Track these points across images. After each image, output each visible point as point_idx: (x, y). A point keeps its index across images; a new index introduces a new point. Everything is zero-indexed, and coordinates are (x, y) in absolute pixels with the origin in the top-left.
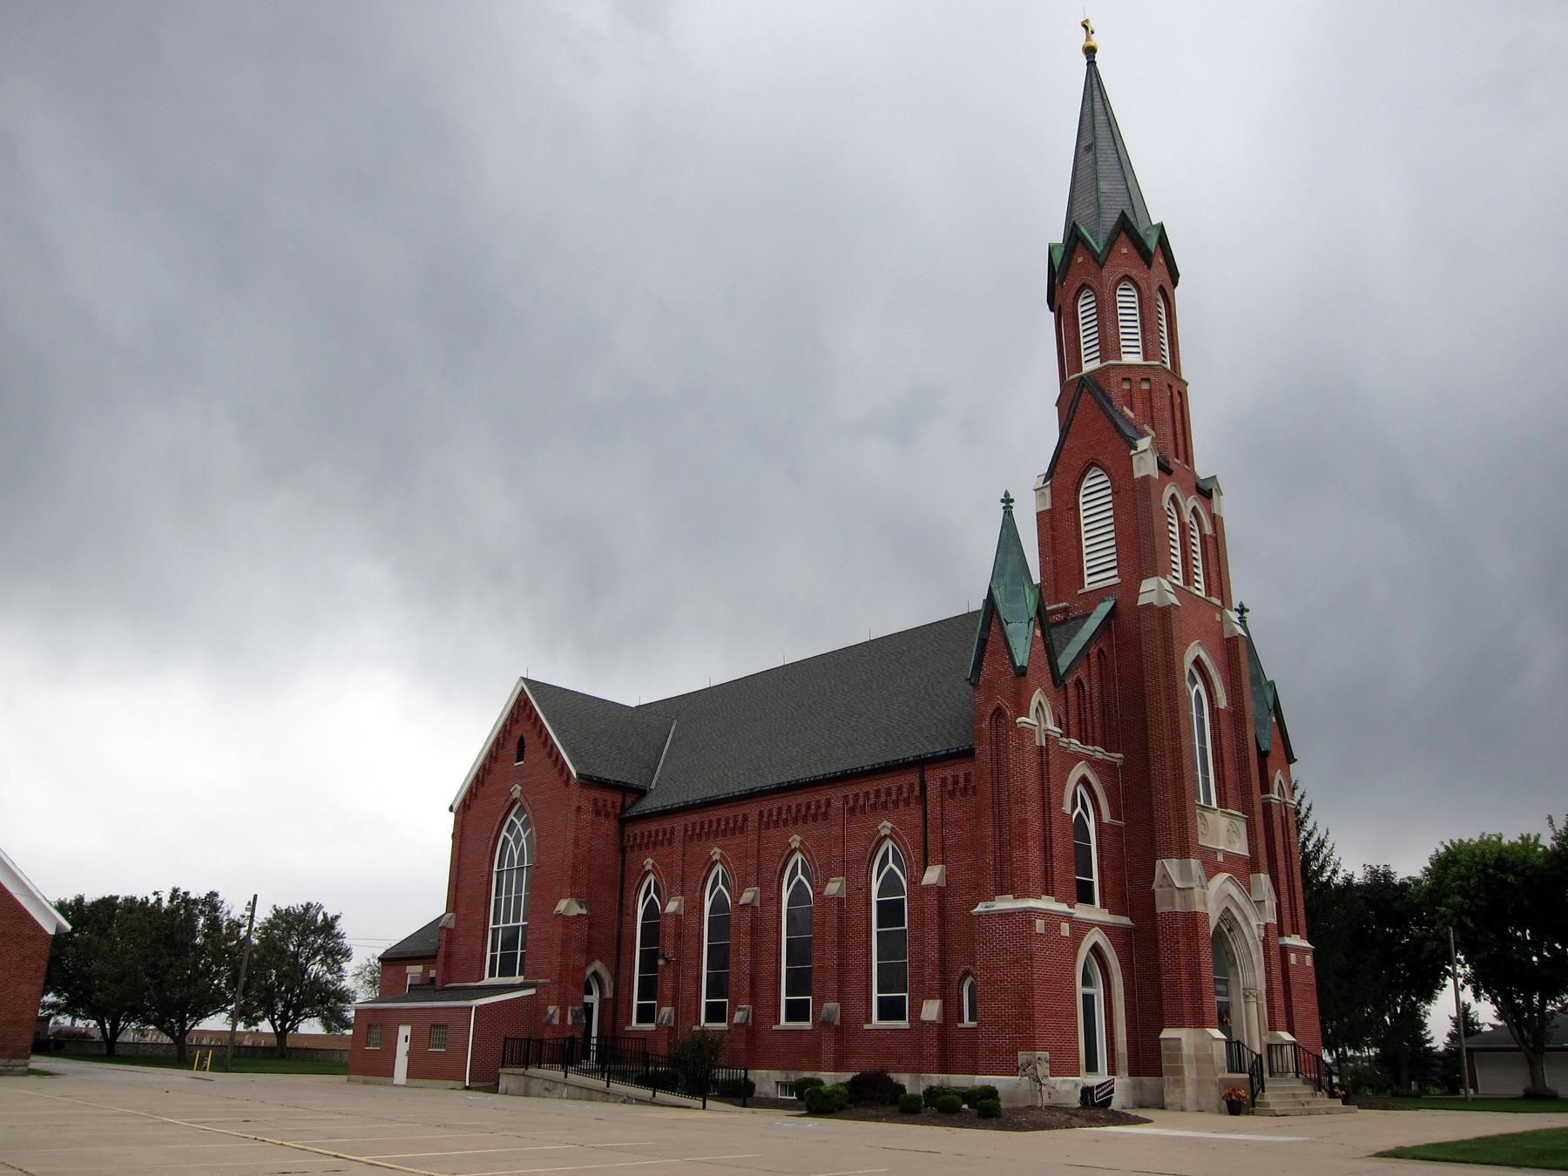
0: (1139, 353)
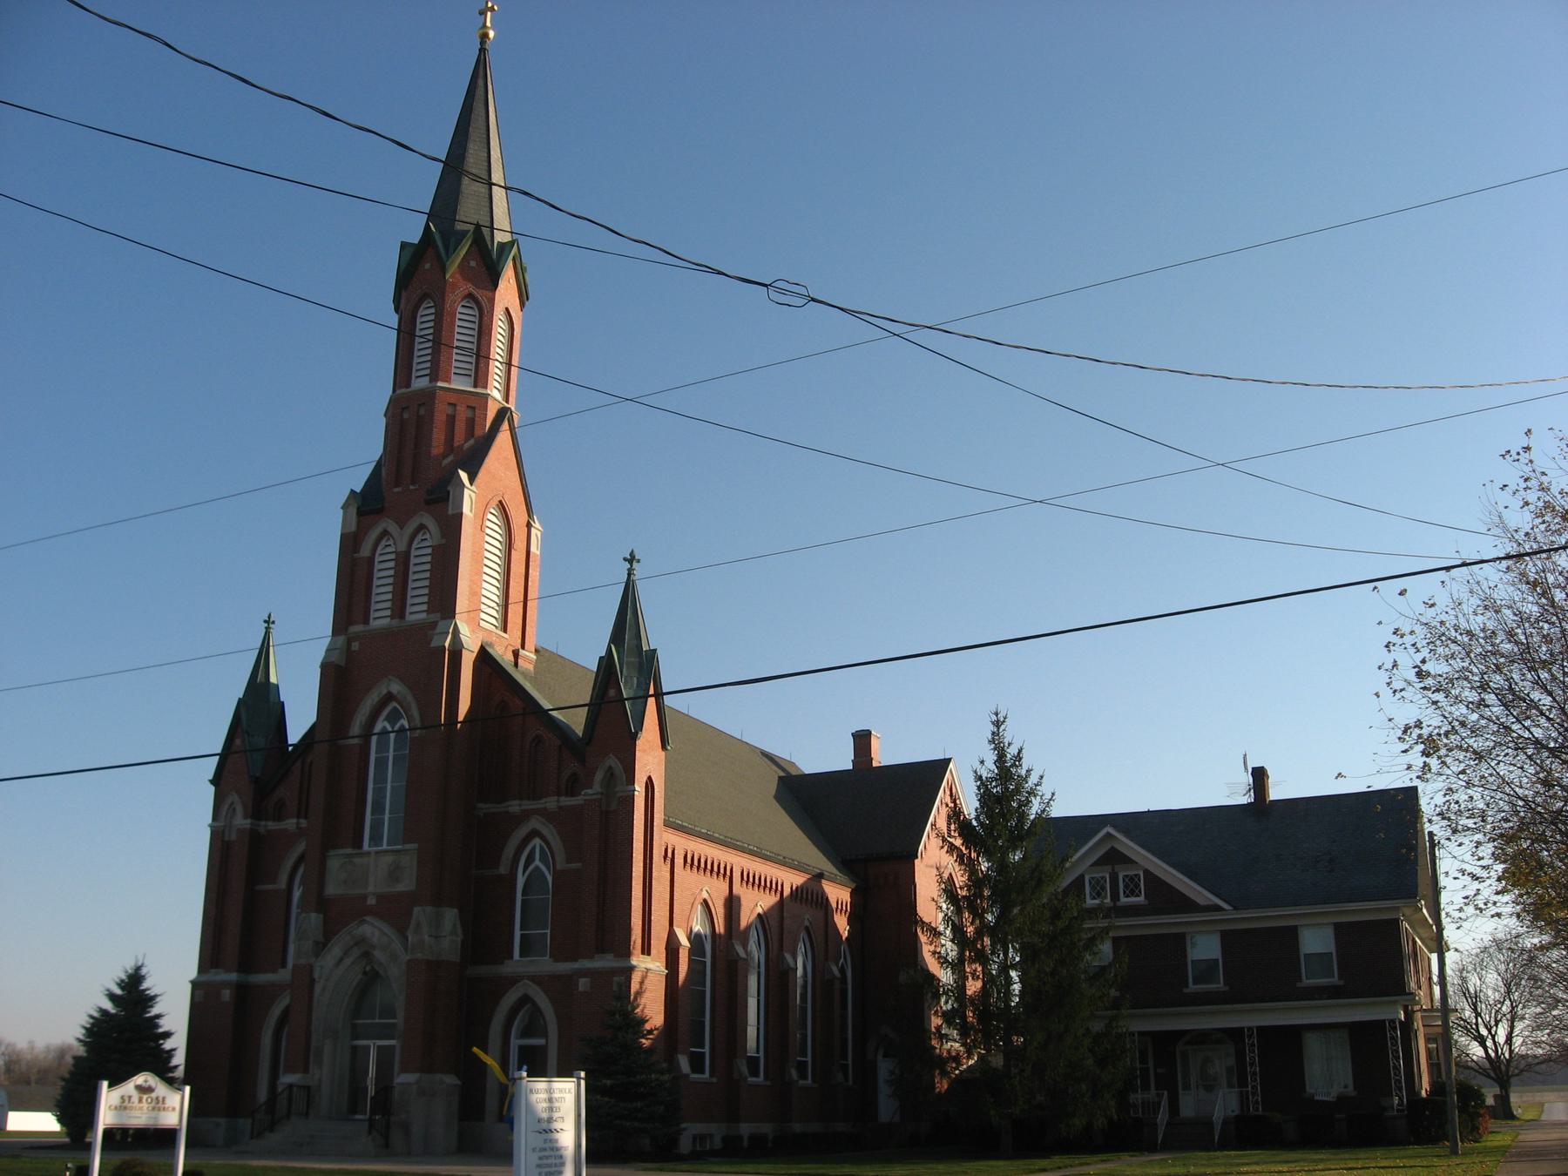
0: (470, 376)
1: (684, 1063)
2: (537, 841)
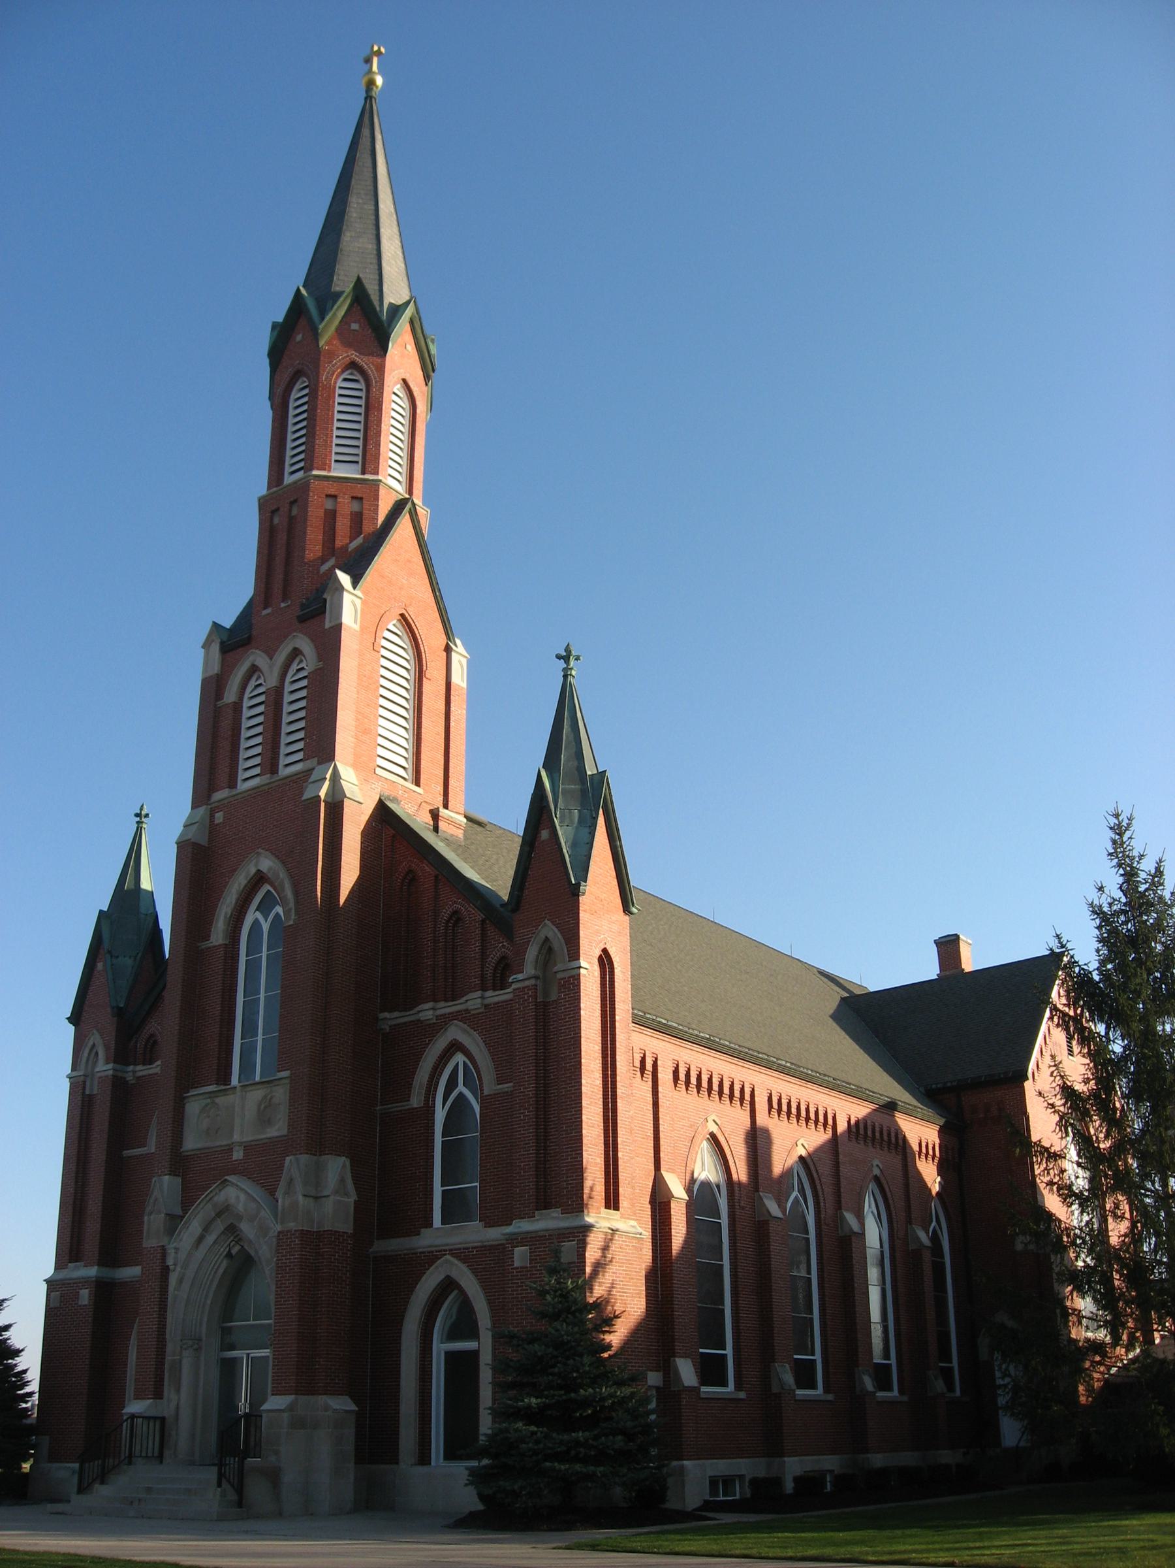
0: (357, 462)
1: (687, 1372)
2: (460, 1058)
